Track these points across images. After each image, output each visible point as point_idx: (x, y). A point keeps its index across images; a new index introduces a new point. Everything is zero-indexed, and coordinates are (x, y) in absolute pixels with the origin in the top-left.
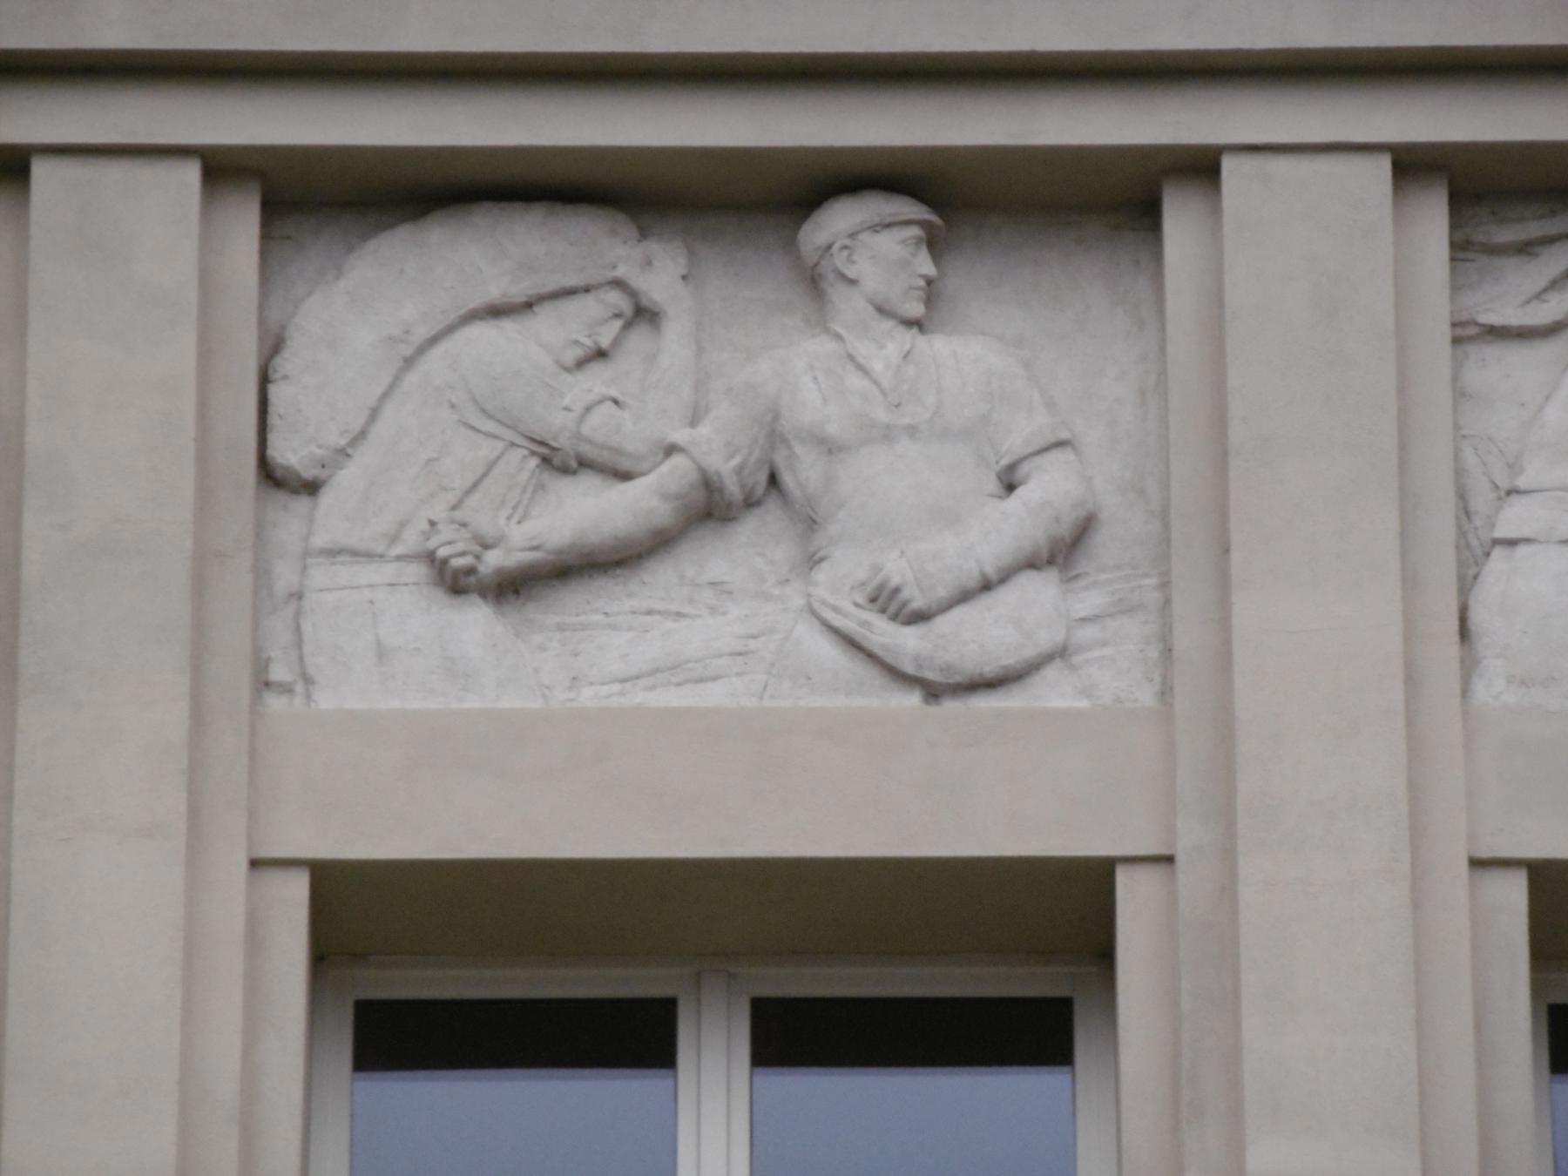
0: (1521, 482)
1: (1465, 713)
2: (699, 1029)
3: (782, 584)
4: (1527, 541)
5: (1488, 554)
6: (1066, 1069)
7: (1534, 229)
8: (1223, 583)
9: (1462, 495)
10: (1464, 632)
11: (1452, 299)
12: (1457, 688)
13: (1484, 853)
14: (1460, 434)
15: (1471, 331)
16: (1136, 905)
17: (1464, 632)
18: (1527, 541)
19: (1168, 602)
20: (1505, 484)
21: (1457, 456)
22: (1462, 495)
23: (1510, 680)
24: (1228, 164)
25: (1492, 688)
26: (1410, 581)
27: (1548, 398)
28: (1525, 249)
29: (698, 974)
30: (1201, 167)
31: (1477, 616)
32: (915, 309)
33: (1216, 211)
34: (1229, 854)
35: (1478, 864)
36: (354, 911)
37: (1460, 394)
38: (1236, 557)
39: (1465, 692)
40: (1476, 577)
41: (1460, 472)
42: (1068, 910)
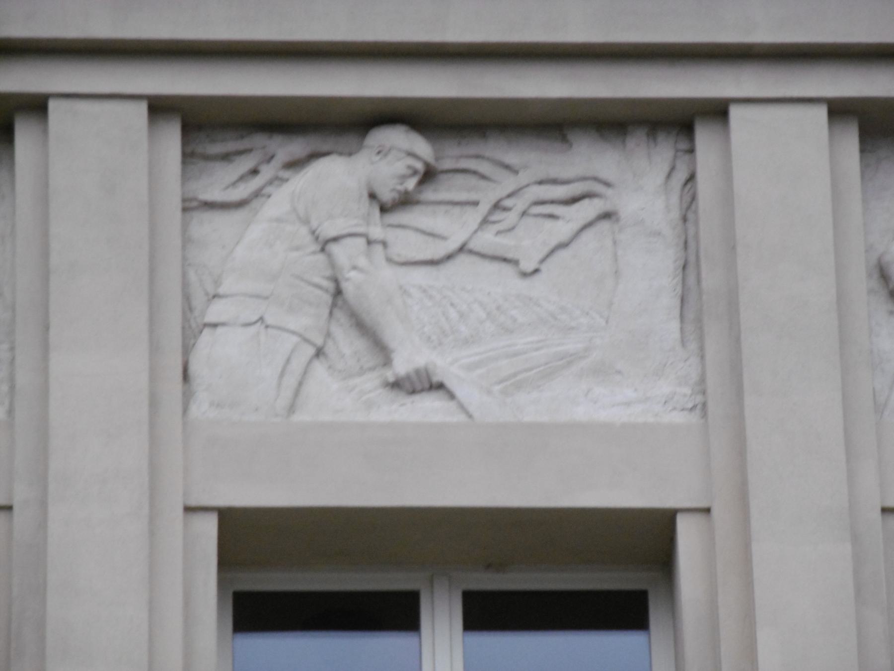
0: (221, 291)
1: (185, 424)
2: (433, 609)
4: (223, 324)
5: (201, 332)
7: (231, 146)
8: (45, 348)
9: (187, 298)
10: (186, 376)
11: (183, 183)
12: (179, 409)
13: (193, 503)
14: (185, 262)
15: (195, 204)
16: (688, 537)
17: (186, 376)
18: (223, 324)
19: (13, 359)
20: (212, 291)
21: (184, 275)
22: (187, 298)
23: (212, 404)
24: (52, 105)
25: (201, 409)
26: (155, 348)
27: (238, 243)
28: (226, 157)
31: (193, 368)
33: (45, 131)
34: (43, 504)
35: (189, 510)
36: (243, 535)
37: (186, 241)
38: (52, 332)
39: (185, 410)
40: (194, 345)
41: (185, 285)
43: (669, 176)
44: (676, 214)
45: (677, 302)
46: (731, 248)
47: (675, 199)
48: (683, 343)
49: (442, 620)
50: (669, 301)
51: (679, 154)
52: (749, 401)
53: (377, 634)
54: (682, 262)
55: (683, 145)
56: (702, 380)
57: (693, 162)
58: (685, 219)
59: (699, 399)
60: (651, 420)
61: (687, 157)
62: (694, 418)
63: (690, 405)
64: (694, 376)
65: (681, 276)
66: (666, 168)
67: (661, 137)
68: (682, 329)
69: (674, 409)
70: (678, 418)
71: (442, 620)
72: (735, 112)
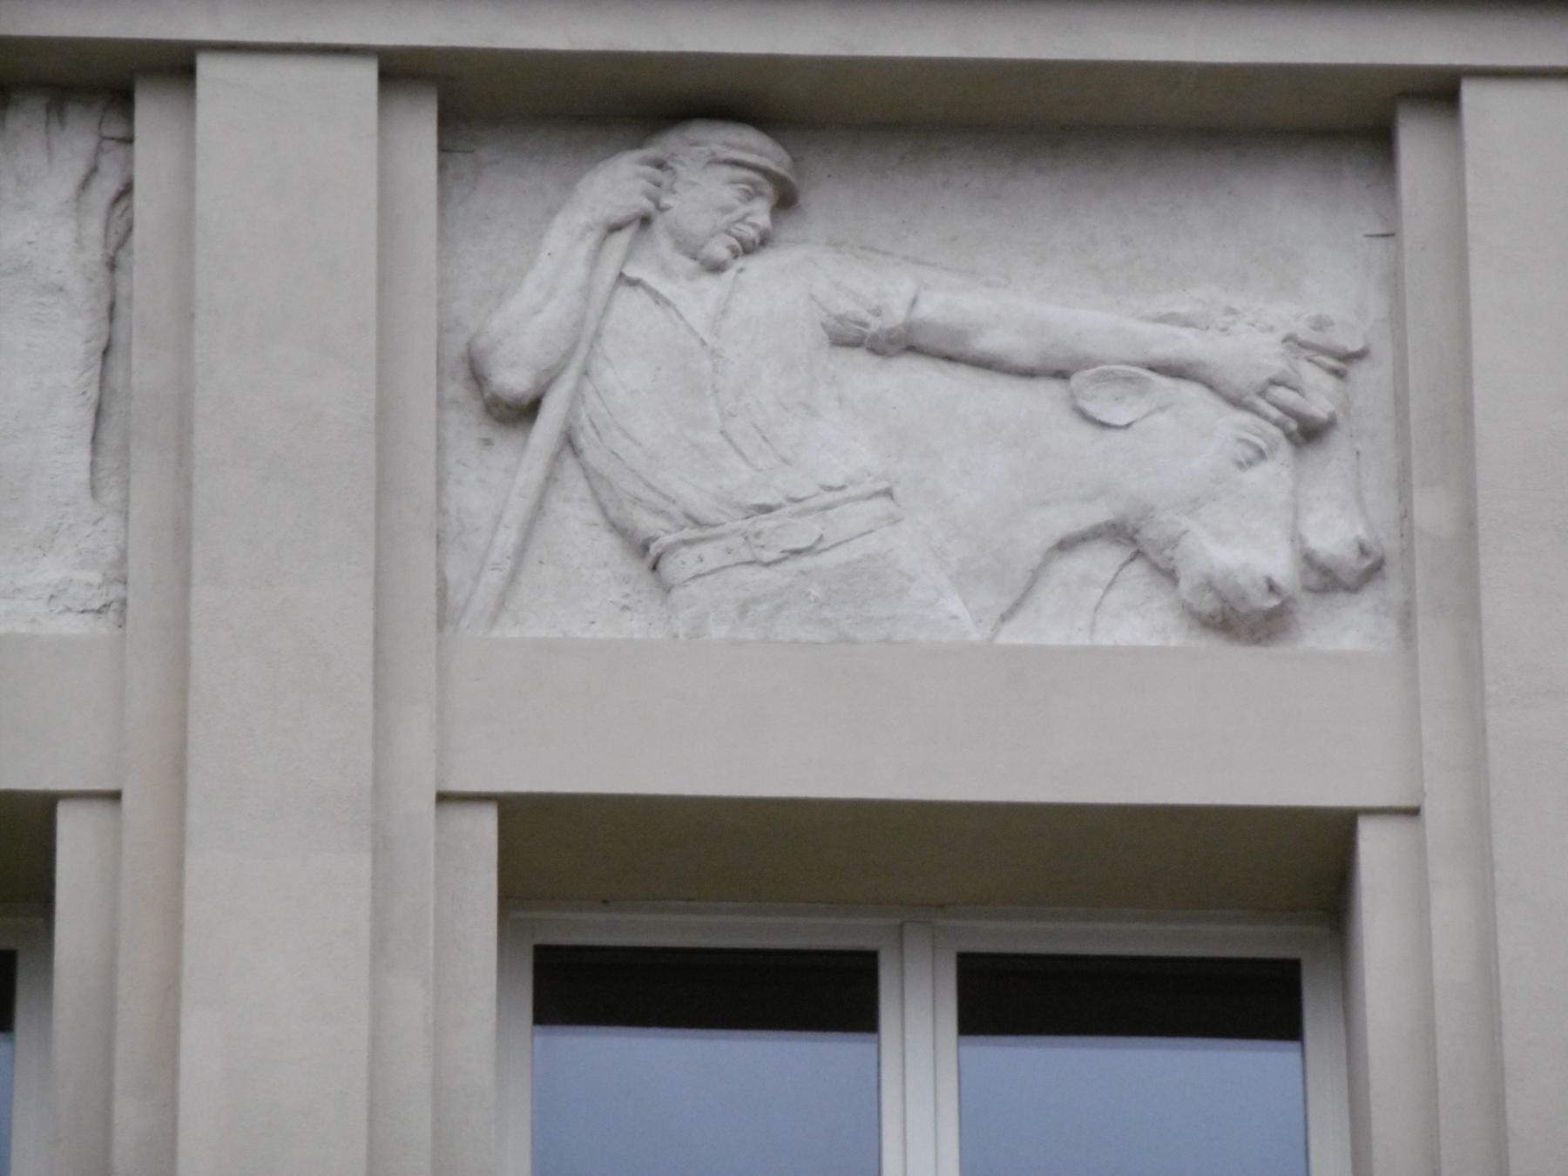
3: (918, 504)
6: (1293, 1046)
29: (901, 926)
30: (1440, 92)
32: (719, 249)
36: (547, 843)
42: (1308, 863)
43: (85, 185)
44: (94, 255)
45: (88, 416)
46: (186, 314)
47: (94, 227)
48: (94, 490)
49: (918, 1008)
50: (74, 414)
51: (107, 144)
52: (201, 593)
53: (653, 1030)
54: (102, 343)
55: (115, 129)
56: (123, 559)
57: (129, 161)
58: (112, 265)
59: (116, 591)
60: (22, 629)
61: (120, 151)
62: (103, 628)
63: (96, 605)
64: (111, 553)
65: (97, 370)
66: (79, 168)
67: (73, 113)
68: (93, 466)
69: (69, 610)
70: (73, 626)
71: (918, 1008)
72: (207, 67)
